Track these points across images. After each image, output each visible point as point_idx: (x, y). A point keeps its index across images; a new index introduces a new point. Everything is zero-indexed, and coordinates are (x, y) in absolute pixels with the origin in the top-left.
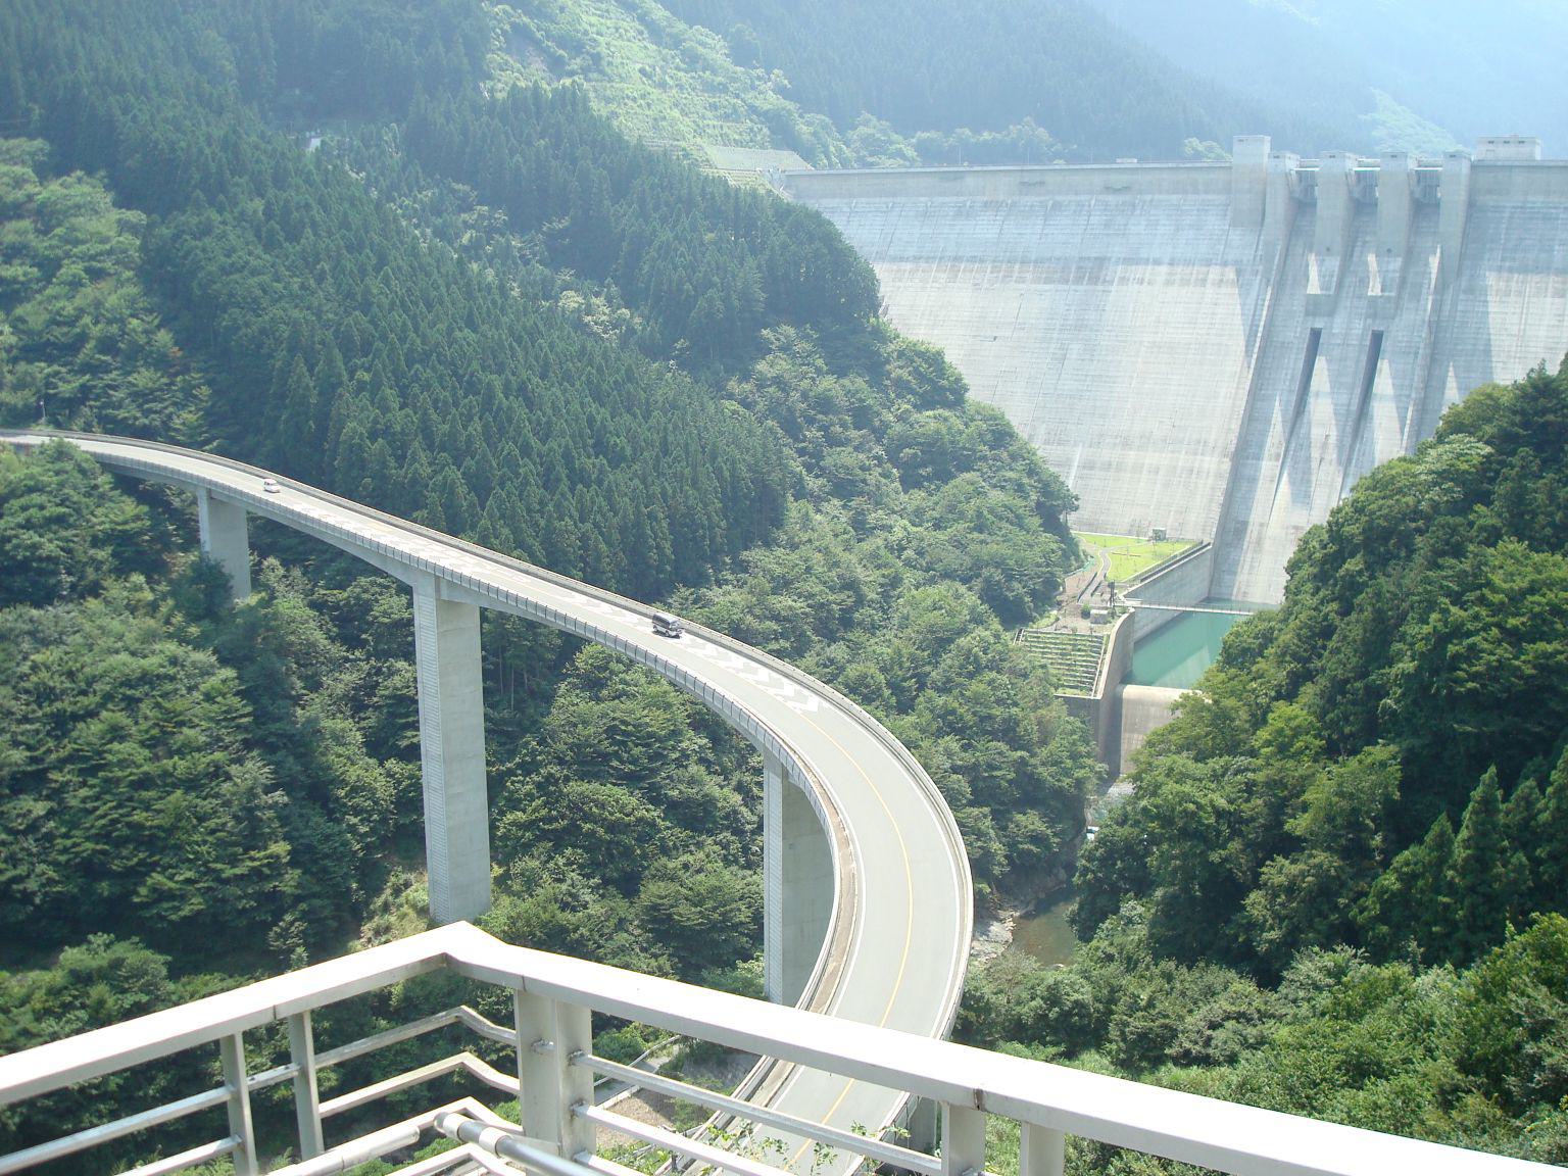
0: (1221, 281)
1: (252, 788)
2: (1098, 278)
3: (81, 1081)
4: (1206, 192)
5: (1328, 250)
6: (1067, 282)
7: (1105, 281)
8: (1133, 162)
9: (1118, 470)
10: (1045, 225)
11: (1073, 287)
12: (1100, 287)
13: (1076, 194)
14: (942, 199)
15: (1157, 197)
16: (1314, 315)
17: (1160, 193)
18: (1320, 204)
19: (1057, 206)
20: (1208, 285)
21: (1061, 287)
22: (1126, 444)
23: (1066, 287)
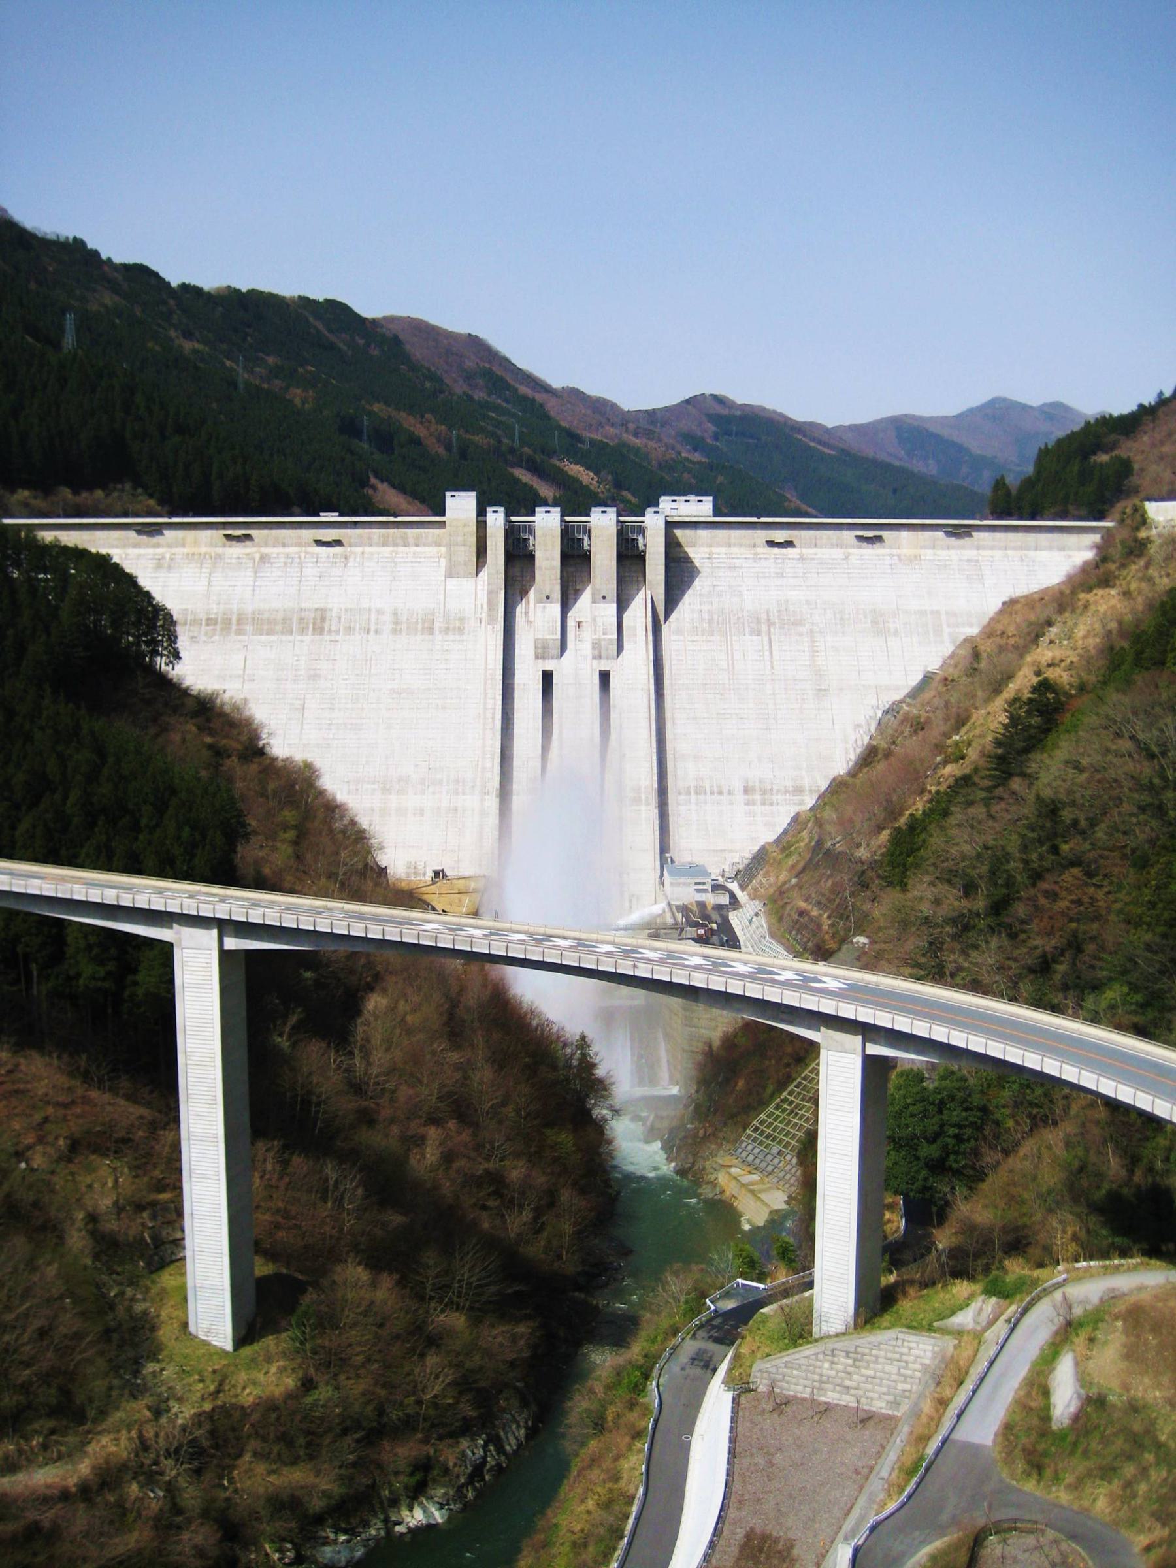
0: (448, 628)
1: (820, 843)
2: (322, 629)
3: (537, 1003)
4: (417, 545)
5: (548, 597)
6: (291, 633)
7: (330, 631)
8: (333, 517)
9: (730, 793)
10: (256, 577)
11: (299, 638)
12: (326, 637)
13: (284, 545)
14: (137, 551)
15: (368, 549)
16: (543, 658)
17: (371, 545)
18: (538, 554)
19: (263, 558)
20: (436, 632)
21: (284, 638)
22: (386, 790)
23: (290, 638)
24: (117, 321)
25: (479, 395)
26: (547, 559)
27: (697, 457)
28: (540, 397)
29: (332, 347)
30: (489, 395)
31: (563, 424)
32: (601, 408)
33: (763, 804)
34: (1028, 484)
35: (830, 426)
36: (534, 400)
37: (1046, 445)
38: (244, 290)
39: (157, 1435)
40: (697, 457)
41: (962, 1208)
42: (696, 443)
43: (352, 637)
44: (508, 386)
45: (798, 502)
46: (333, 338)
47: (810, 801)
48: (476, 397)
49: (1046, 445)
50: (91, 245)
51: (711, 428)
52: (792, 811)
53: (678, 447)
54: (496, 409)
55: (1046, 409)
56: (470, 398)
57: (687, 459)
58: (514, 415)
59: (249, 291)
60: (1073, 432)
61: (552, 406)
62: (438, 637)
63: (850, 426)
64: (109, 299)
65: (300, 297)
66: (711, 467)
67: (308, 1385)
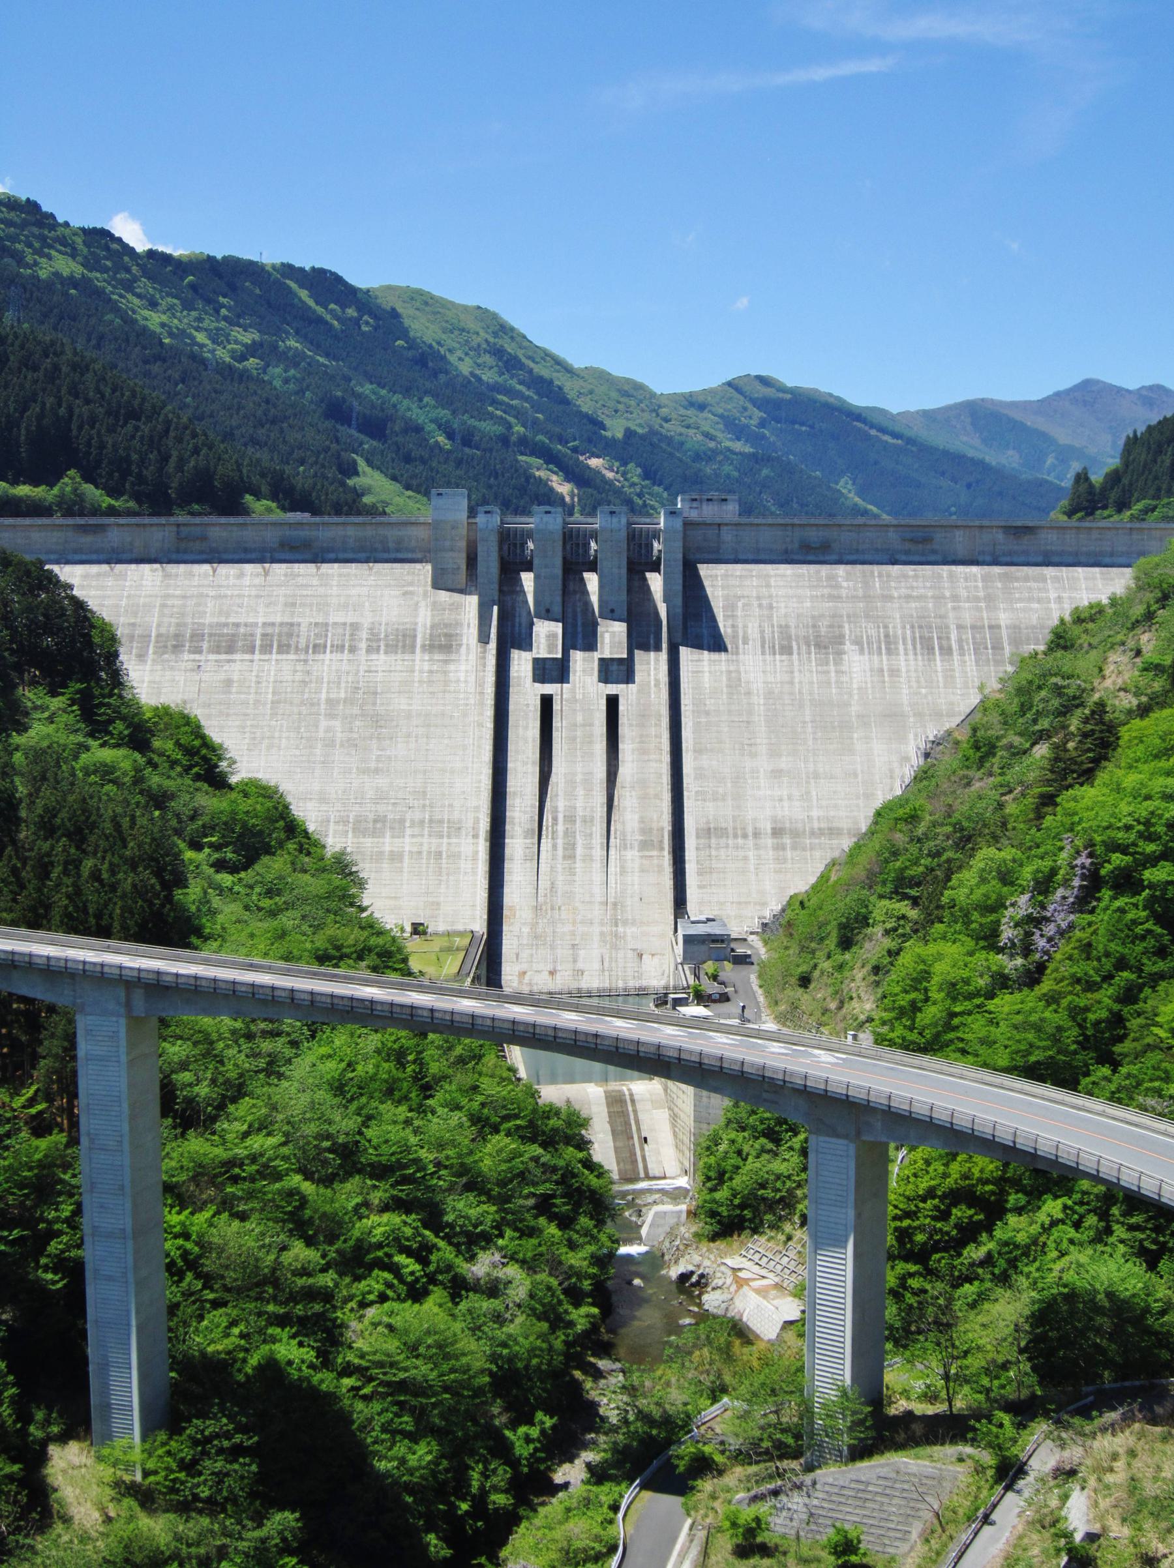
20: (418, 649)
24: (73, 291)
25: (489, 376)
26: (546, 566)
27: (738, 446)
28: (560, 379)
29: (320, 320)
30: (501, 374)
31: (584, 409)
32: (631, 392)
33: (794, 848)
34: (1114, 478)
35: (895, 412)
36: (551, 382)
37: (1135, 432)
38: (219, 257)
39: (896, 1207)
40: (738, 446)
41: (778, 1521)
42: (737, 430)
43: (321, 656)
44: (522, 366)
45: (857, 499)
46: (320, 310)
47: (847, 843)
48: (484, 378)
49: (1135, 432)
50: (46, 208)
51: (758, 414)
52: (829, 856)
53: (719, 435)
54: (509, 392)
55: (1144, 393)
56: (479, 379)
57: (728, 449)
58: (527, 399)
59: (224, 258)
60: (1165, 419)
61: (571, 388)
62: (362, 654)
63: (917, 412)
64: (65, 266)
65: (283, 264)
66: (754, 457)
67: (1006, 1165)
